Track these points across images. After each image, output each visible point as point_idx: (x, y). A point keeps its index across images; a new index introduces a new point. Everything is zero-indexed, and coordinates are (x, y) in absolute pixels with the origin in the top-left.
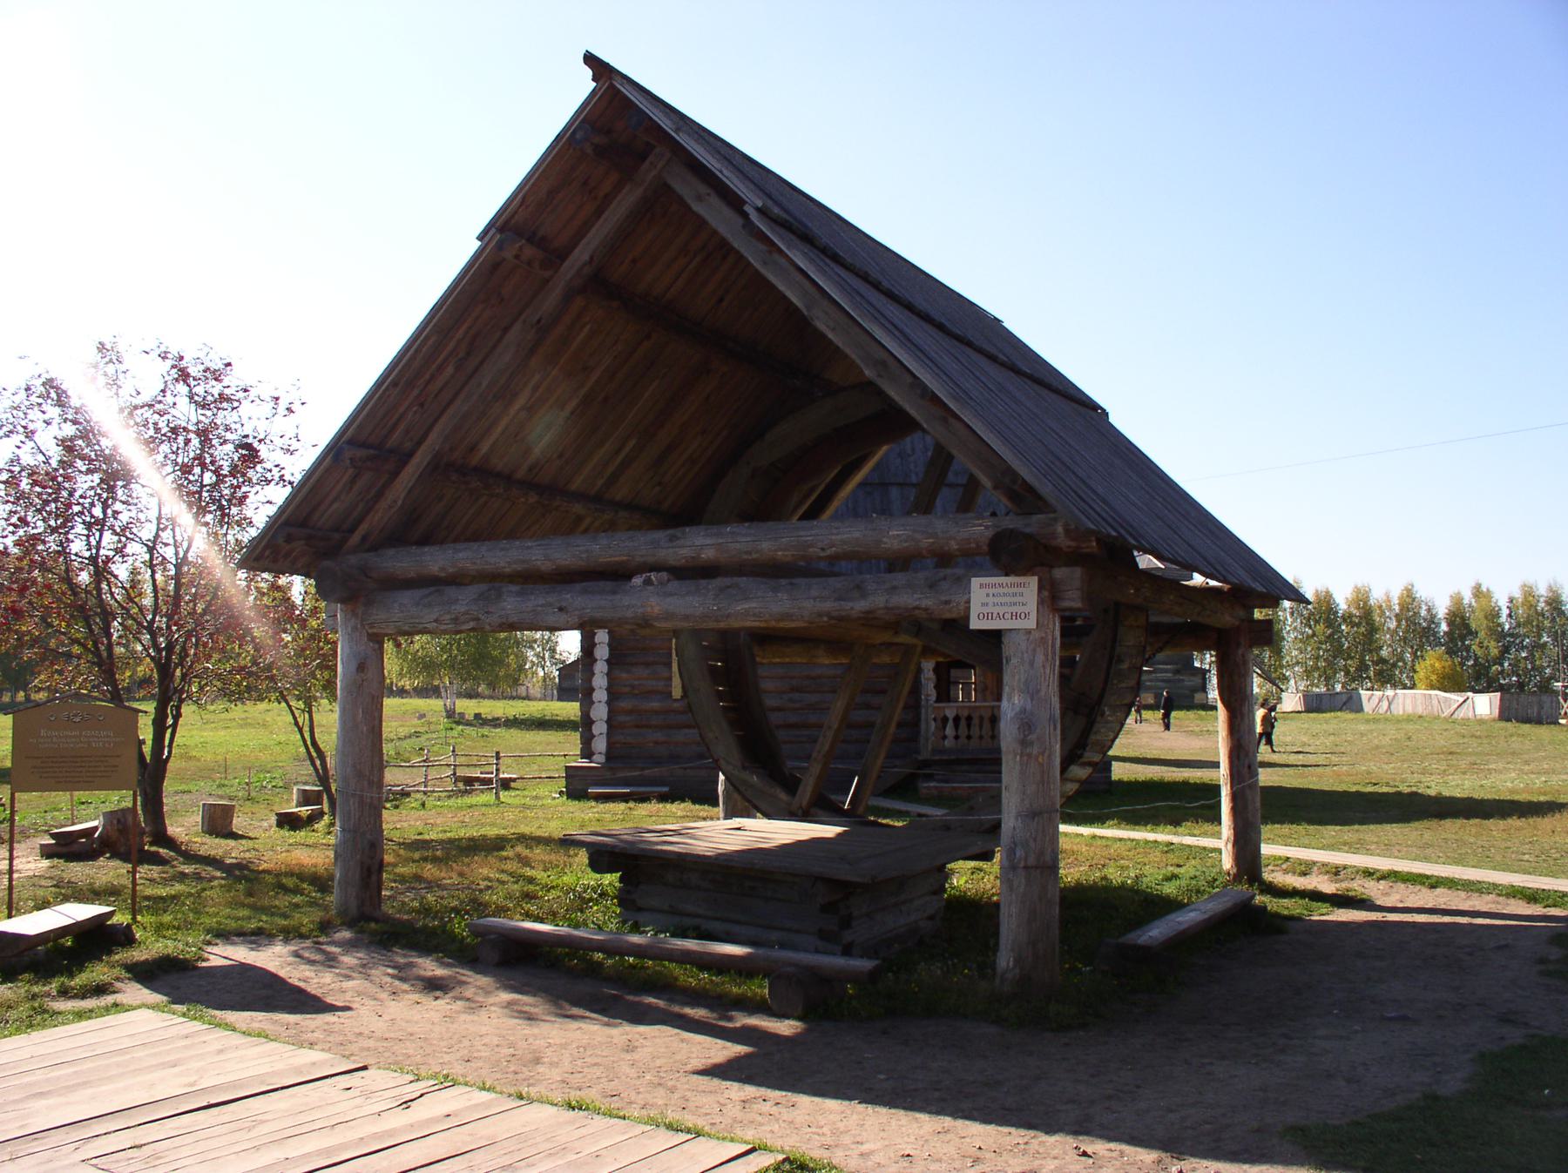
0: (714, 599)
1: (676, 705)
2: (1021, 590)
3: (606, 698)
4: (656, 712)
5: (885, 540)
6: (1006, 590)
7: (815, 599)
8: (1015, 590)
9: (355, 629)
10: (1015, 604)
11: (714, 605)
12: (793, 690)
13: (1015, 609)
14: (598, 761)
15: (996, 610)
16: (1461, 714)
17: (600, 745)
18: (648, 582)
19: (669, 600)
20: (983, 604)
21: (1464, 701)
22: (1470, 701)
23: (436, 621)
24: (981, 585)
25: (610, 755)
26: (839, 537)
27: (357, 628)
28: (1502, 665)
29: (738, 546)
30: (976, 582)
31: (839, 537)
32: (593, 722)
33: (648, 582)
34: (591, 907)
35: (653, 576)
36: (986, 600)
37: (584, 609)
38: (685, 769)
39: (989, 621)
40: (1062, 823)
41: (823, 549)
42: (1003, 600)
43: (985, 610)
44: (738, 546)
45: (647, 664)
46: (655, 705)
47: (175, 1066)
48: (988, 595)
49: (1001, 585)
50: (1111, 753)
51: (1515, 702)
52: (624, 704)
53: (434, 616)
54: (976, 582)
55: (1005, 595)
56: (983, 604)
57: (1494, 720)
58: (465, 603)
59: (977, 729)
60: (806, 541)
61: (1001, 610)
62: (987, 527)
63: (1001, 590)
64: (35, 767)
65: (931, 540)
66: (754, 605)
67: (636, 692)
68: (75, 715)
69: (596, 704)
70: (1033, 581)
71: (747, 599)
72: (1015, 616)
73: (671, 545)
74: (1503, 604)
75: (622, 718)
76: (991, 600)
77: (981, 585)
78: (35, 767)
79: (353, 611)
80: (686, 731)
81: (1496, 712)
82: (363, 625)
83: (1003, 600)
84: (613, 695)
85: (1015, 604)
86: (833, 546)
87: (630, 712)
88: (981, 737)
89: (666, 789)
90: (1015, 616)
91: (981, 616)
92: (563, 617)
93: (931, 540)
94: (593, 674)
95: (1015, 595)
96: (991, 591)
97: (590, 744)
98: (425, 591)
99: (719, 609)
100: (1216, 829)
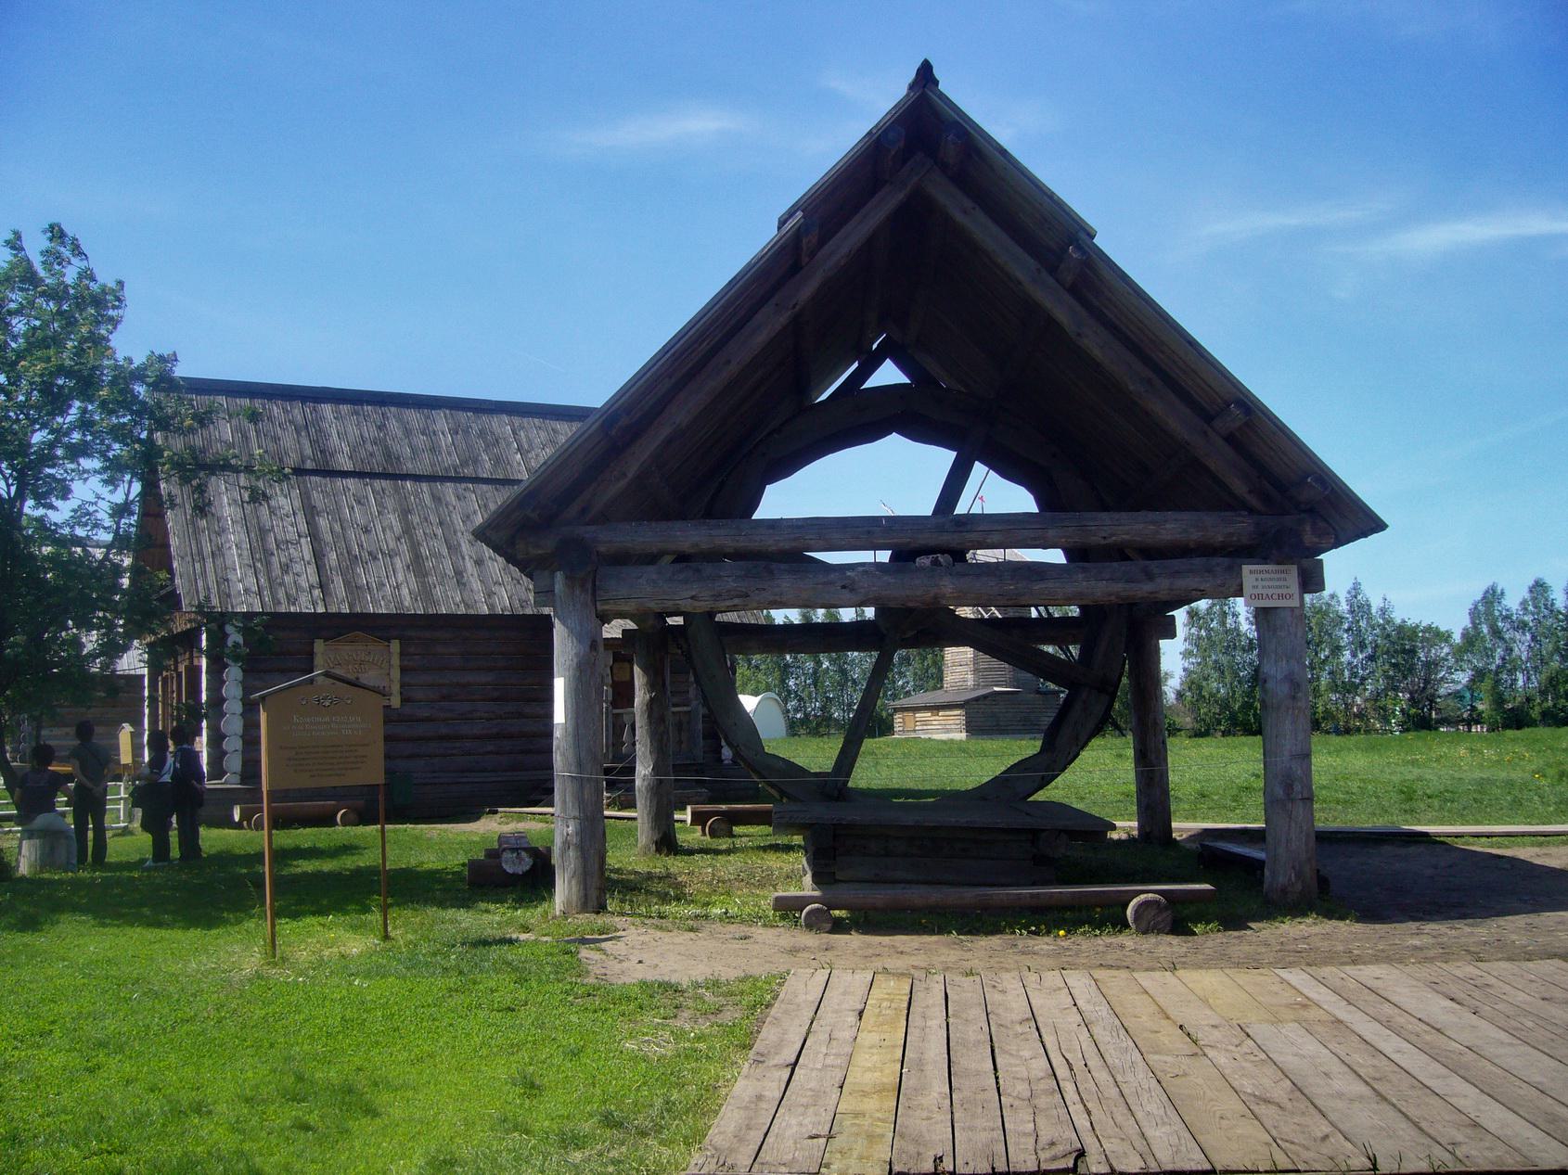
0: (1012, 580)
2: (1283, 575)
3: (241, 710)
8: (1279, 576)
12: (444, 698)
13: (1280, 591)
15: (1264, 592)
20: (1254, 587)
23: (692, 598)
28: (1367, 689)
30: (1246, 569)
32: (225, 753)
33: (936, 563)
34: (873, 1054)
35: (941, 558)
36: (1255, 584)
41: (1105, 538)
42: (1271, 583)
43: (1256, 592)
47: (1340, 1022)
48: (1257, 580)
50: (1126, 826)
54: (1246, 569)
56: (1254, 587)
61: (1270, 592)
63: (1268, 576)
64: (290, 759)
68: (325, 699)
70: (1294, 569)
72: (1281, 597)
74: (101, 465)
76: (1260, 584)
78: (290, 759)
83: (1271, 583)
86: (1114, 535)
90: (1281, 597)
92: (846, 594)
95: (1279, 579)
96: (1260, 576)
99: (1016, 589)
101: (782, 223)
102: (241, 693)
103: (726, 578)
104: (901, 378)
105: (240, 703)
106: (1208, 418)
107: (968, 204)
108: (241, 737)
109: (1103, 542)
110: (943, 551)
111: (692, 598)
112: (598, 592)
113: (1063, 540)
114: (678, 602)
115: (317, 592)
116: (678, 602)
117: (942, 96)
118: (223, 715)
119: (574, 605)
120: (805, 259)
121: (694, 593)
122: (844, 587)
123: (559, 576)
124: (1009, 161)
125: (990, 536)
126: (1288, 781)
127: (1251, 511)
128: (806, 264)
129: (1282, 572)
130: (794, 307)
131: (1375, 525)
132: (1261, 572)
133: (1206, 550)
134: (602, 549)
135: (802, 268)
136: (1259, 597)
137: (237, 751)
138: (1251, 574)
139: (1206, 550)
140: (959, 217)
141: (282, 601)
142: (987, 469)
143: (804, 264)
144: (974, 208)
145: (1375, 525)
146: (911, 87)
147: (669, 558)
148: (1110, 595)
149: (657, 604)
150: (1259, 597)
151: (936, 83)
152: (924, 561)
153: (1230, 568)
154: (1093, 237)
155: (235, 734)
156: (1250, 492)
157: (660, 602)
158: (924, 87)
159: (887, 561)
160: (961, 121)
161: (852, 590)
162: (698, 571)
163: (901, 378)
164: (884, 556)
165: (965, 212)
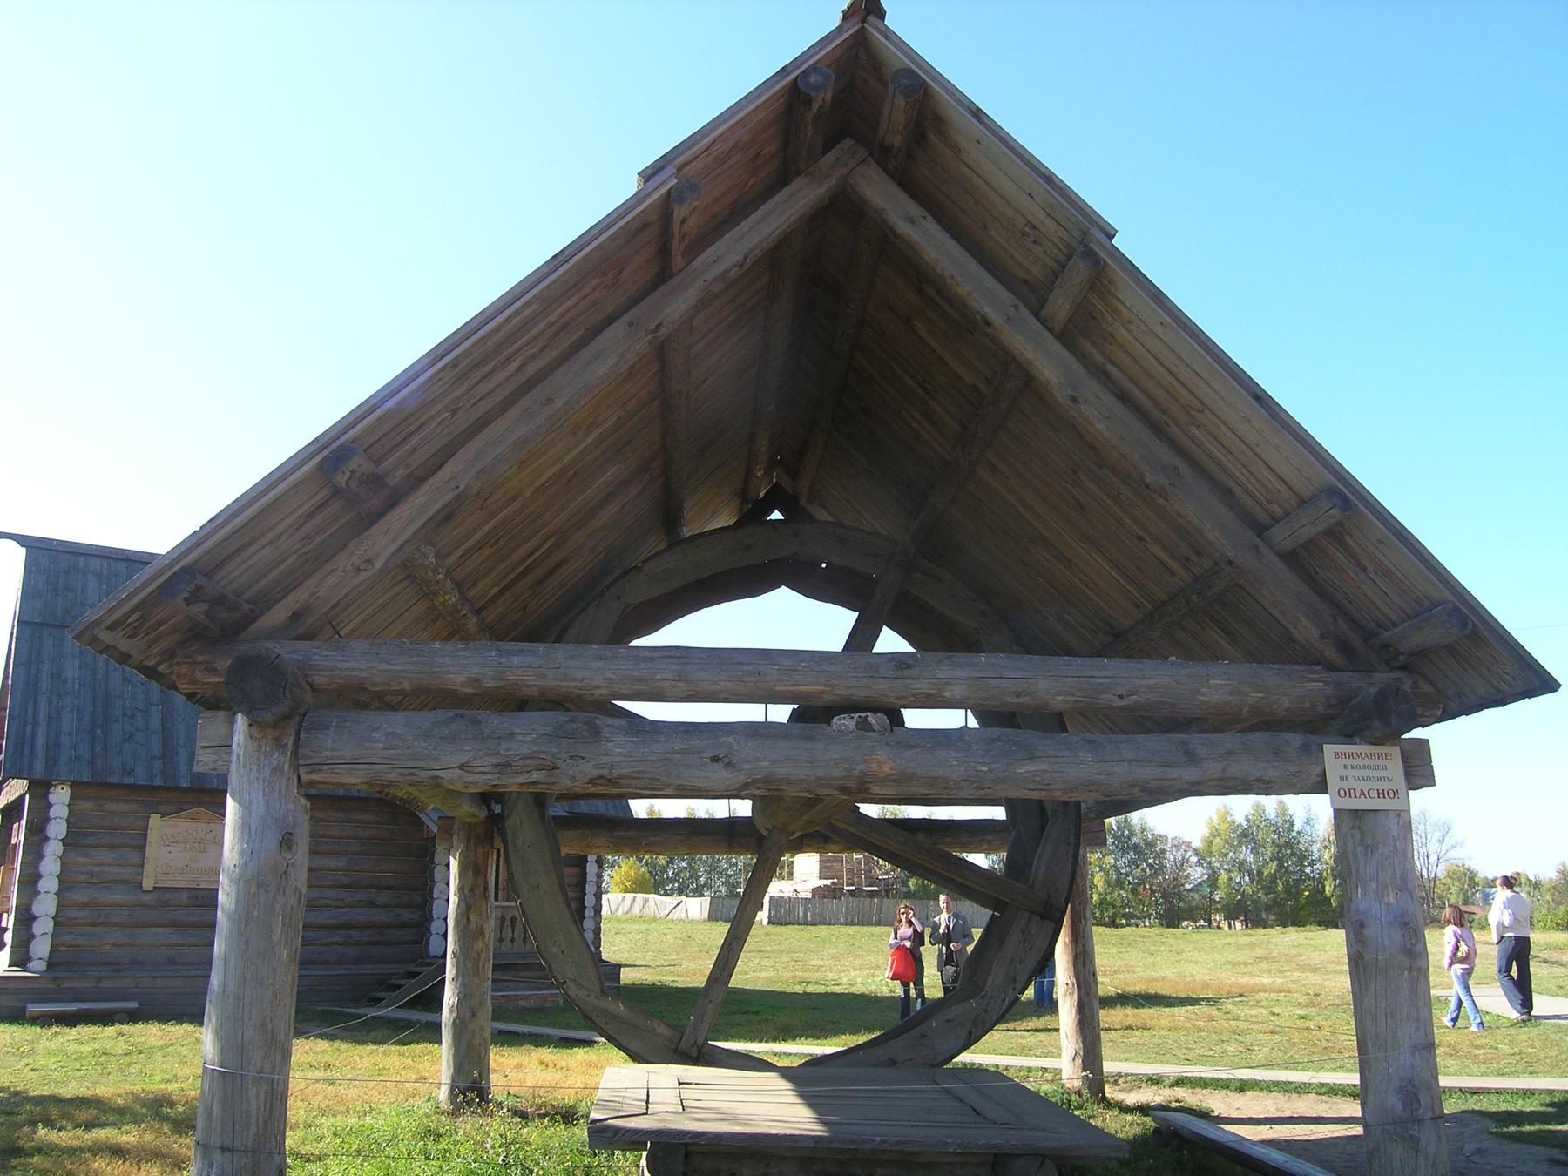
1: (146, 898)
4: (118, 906)
5: (1203, 690)
6: (1367, 762)
7: (1130, 762)
9: (277, 770)
10: (1379, 779)
11: (984, 764)
14: (38, 966)
15: (1358, 786)
16: (677, 914)
17: (41, 948)
18: (864, 726)
19: (907, 754)
20: (1341, 778)
21: (679, 904)
22: (683, 903)
23: (461, 767)
24: (1336, 754)
25: (51, 964)
26: (1145, 682)
27: (282, 770)
29: (1003, 684)
30: (1329, 750)
31: (1145, 682)
32: (34, 918)
33: (864, 726)
35: (872, 718)
36: (1344, 773)
37: (758, 760)
38: (155, 978)
39: (1353, 799)
40: (137, 1008)
41: (1120, 697)
42: (1366, 773)
43: (1346, 785)
44: (1003, 684)
45: (112, 847)
46: (118, 897)
49: (1359, 755)
51: (721, 905)
52: (80, 896)
53: (463, 759)
54: (1329, 750)
55: (1365, 767)
56: (1341, 778)
57: (704, 921)
58: (529, 738)
59: (510, 930)
60: (1100, 684)
61: (1366, 786)
62: (1326, 684)
63: (1360, 762)
65: (1261, 695)
66: (1043, 767)
67: (94, 880)
69: (42, 895)
71: (1033, 758)
72: (1382, 794)
73: (899, 673)
75: (72, 914)
76: (1350, 773)
77: (1336, 754)
79: (276, 740)
80: (155, 930)
81: (706, 915)
82: (296, 767)
83: (1366, 773)
84: (66, 883)
85: (1379, 779)
87: (85, 906)
88: (512, 941)
89: (133, 1005)
91: (1391, 795)
92: (719, 774)
93: (1261, 695)
94: (41, 857)
95: (1377, 768)
96: (1349, 762)
97: (28, 946)
98: (442, 714)
99: (990, 771)
100: (430, 1017)
101: (648, 175)
102: (59, 869)
103: (521, 738)
104: (780, 517)
105: (57, 880)
106: (1261, 529)
107: (915, 209)
108: (53, 918)
109: (1118, 703)
110: (875, 710)
111: (461, 767)
112: (301, 751)
113: (1059, 698)
114: (436, 773)
115: (158, 764)
116: (436, 773)
117: (888, 34)
118: (37, 893)
119: (259, 771)
120: (678, 261)
121: (464, 760)
122: (715, 759)
123: (241, 721)
124: (987, 127)
125: (950, 687)
126: (1410, 1088)
127: (1332, 667)
128: (680, 271)
129: (1380, 756)
130: (658, 327)
131: (1542, 683)
132: (1351, 755)
133: (1268, 722)
134: (319, 680)
135: (672, 277)
136: (1350, 793)
137: (47, 934)
138: (1335, 757)
139: (1268, 722)
140: (903, 228)
141: (117, 772)
142: (769, 720)
143: (675, 270)
144: (924, 218)
145: (1542, 683)
146: (847, 15)
147: (1167, 1082)
148: (1132, 786)
149: (401, 774)
150: (1350, 793)
151: (881, 15)
152: (846, 722)
153: (1305, 748)
154: (1111, 237)
155: (47, 915)
156: (1323, 636)
157: (407, 771)
158: (864, 21)
159: (786, 722)
160: (914, 67)
161: (728, 765)
162: (476, 722)
163: (780, 517)
164: (781, 713)
165: (913, 222)
